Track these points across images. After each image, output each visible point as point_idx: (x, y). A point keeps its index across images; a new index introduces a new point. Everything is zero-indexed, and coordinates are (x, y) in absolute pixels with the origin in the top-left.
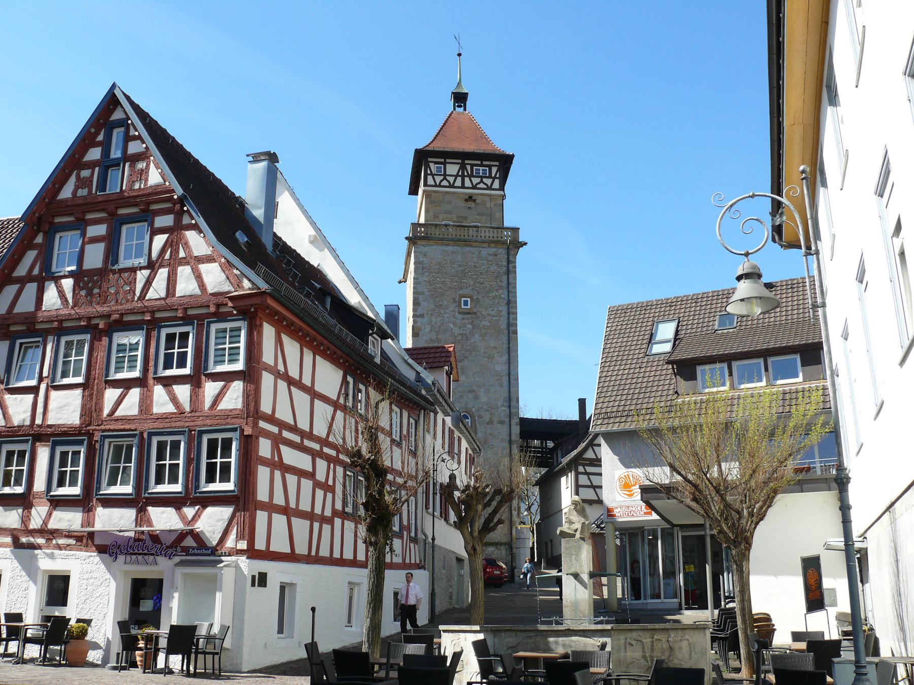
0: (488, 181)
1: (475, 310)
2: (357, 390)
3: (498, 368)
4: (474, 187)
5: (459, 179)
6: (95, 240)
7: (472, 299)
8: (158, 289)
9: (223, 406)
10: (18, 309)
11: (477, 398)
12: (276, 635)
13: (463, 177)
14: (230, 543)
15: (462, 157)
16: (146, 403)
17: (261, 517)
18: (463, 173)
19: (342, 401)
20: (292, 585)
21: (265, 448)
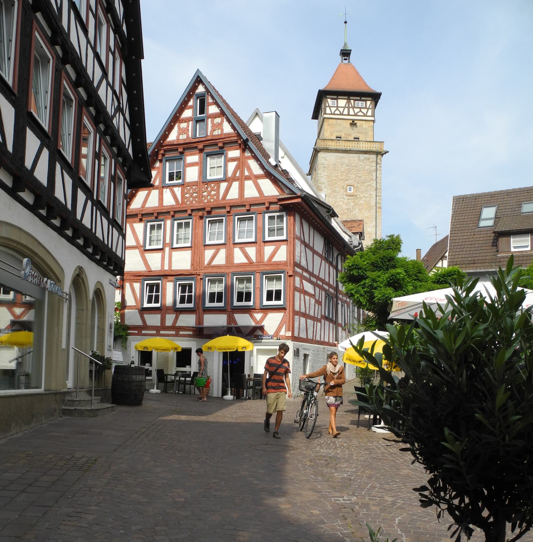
0: (364, 111)
1: (356, 194)
4: (356, 115)
5: (346, 109)
6: (192, 165)
7: (354, 187)
10: (148, 205)
13: (349, 108)
14: (282, 333)
15: (348, 95)
16: (230, 256)
18: (349, 105)
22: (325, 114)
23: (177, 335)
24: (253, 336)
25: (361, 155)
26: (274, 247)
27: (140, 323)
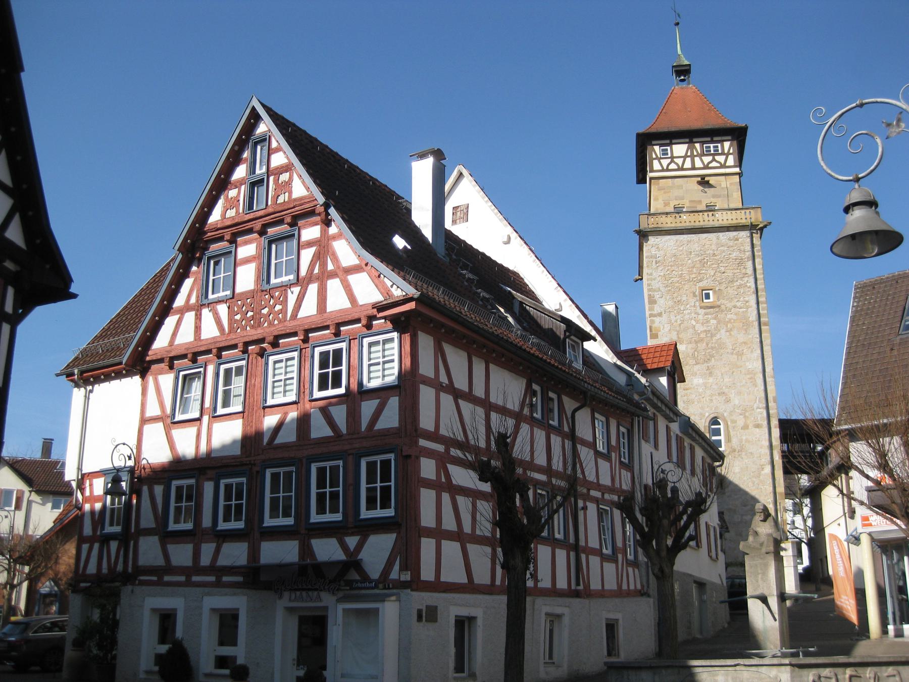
0: (721, 159)
1: (718, 303)
2: (546, 400)
3: (750, 366)
4: (706, 167)
5: (688, 160)
6: (247, 261)
7: (715, 292)
8: (309, 309)
9: (380, 425)
10: (179, 340)
11: (728, 401)
12: (451, 673)
13: (692, 157)
14: (394, 575)
17: (427, 546)
18: (692, 152)
19: (526, 411)
20: (472, 619)
21: (428, 468)
22: (652, 171)
23: (218, 584)
24: (342, 583)
25: (721, 234)
26: (378, 401)
27: (161, 562)
